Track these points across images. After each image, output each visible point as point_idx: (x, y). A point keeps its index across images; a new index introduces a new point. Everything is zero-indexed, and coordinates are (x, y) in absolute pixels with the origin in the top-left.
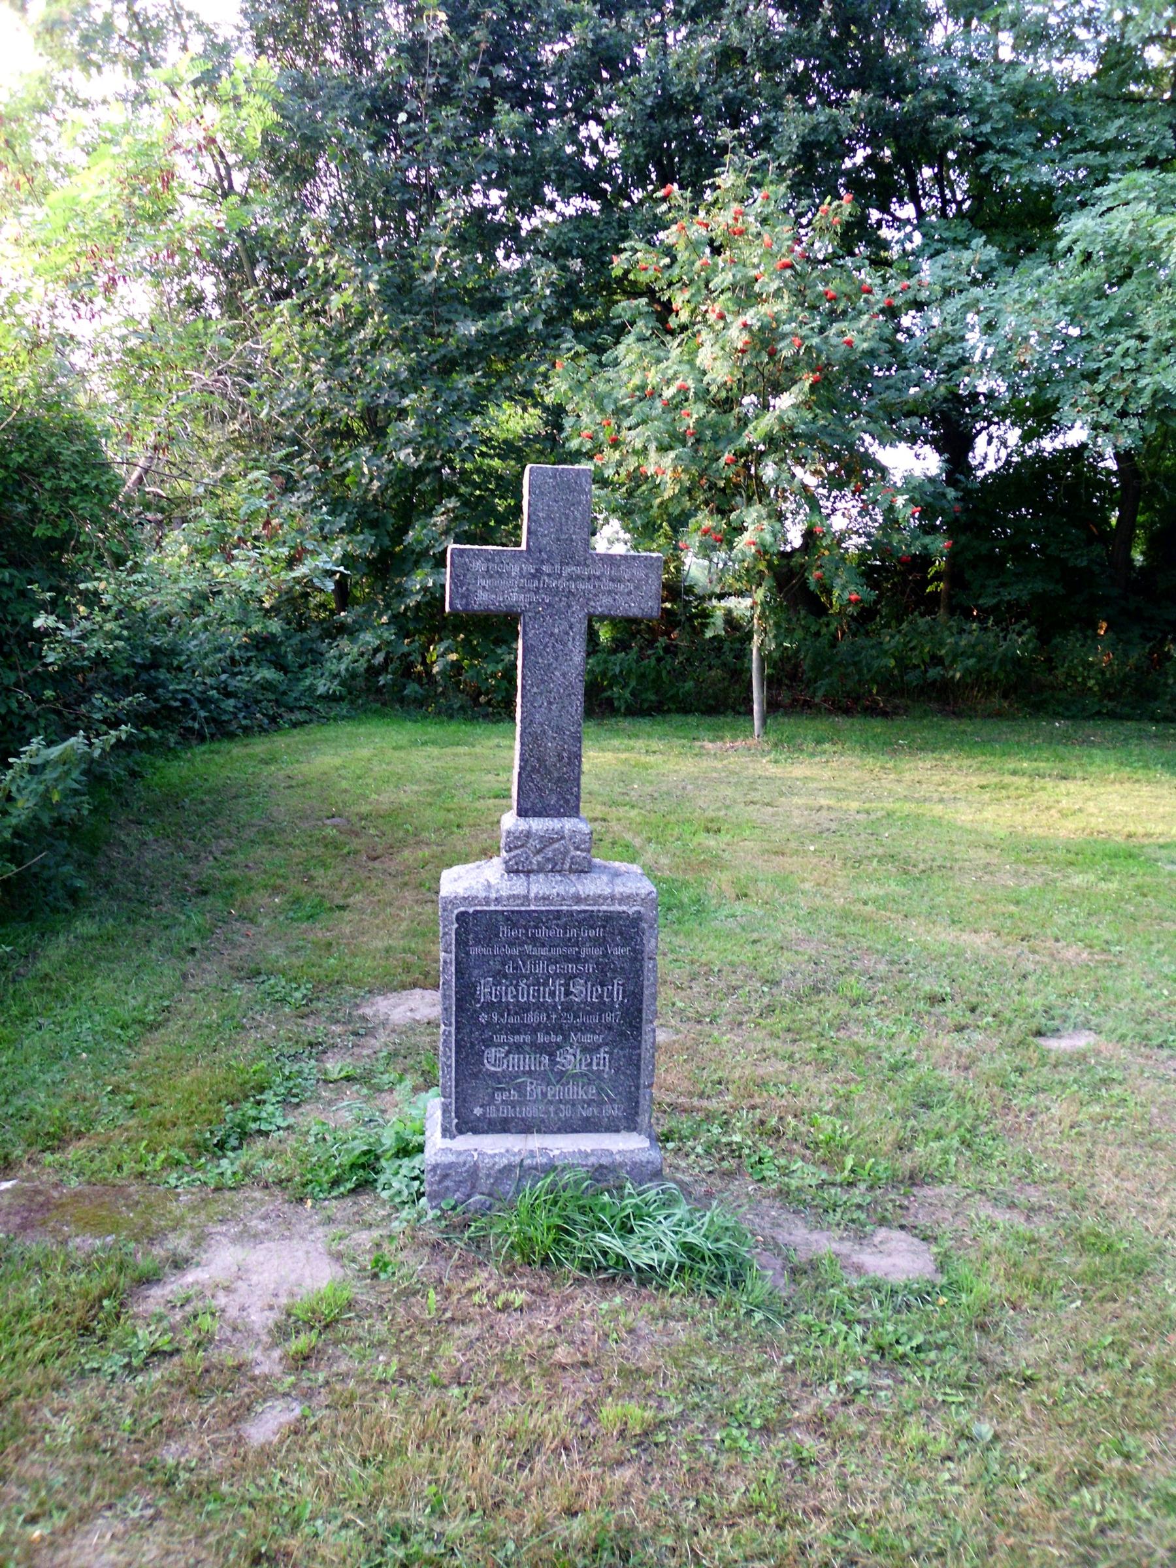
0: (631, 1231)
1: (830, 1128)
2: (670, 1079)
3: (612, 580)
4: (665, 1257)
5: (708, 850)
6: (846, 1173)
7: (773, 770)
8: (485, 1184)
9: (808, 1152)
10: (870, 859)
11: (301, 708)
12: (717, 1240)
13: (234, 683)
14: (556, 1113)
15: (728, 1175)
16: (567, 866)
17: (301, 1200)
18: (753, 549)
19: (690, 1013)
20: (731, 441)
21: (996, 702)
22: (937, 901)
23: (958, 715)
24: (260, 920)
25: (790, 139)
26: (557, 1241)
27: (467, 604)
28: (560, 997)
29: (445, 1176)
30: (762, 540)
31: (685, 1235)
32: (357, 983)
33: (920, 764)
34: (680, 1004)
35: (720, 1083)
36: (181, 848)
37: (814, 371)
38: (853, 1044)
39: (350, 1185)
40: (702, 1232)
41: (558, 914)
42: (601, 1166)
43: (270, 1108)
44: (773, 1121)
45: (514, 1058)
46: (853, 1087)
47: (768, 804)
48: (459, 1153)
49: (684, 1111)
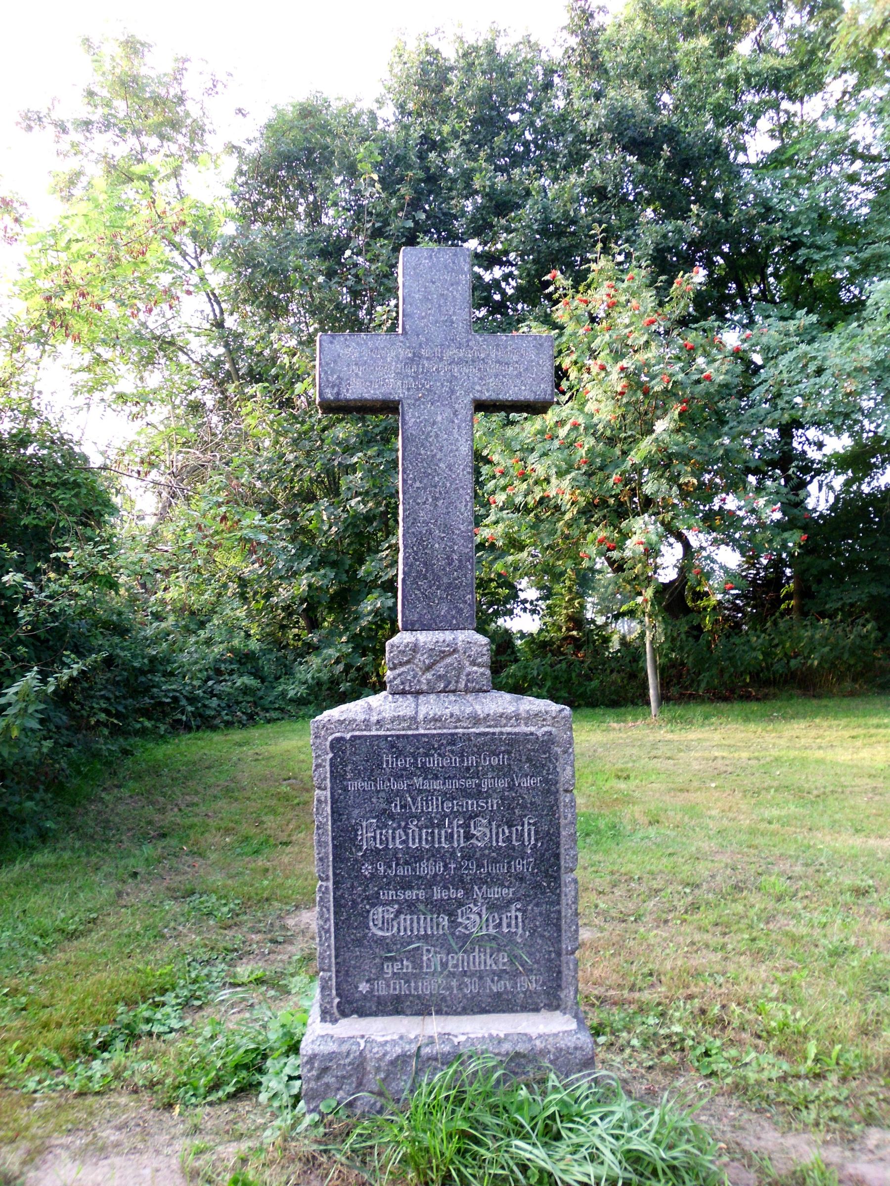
0: (558, 1137)
1: (780, 1015)
2: (597, 973)
3: (498, 362)
4: (603, 1172)
5: (620, 791)
6: (809, 1062)
7: (670, 736)
8: (374, 1080)
9: (760, 1042)
10: (767, 790)
11: (275, 709)
12: (671, 1147)
13: (218, 688)
14: (460, 989)
15: (672, 1071)
16: (462, 686)
17: (169, 1106)
18: (642, 548)
19: (614, 913)
20: (617, 467)
21: (848, 685)
22: (837, 817)
23: (819, 697)
24: (208, 853)
25: (647, 244)
26: (461, 1152)
27: (338, 394)
28: (459, 842)
29: (325, 1070)
30: (649, 539)
31: (629, 1141)
32: (285, 900)
33: (796, 726)
34: (602, 906)
35: (651, 975)
36: (152, 803)
37: (681, 403)
38: (786, 934)
39: (230, 1089)
40: (651, 1135)
41: (453, 739)
42: (518, 1054)
43: (167, 1009)
44: (716, 1010)
45: (405, 919)
46: (794, 973)
47: (669, 758)
48: (342, 1041)
49: (615, 1004)
